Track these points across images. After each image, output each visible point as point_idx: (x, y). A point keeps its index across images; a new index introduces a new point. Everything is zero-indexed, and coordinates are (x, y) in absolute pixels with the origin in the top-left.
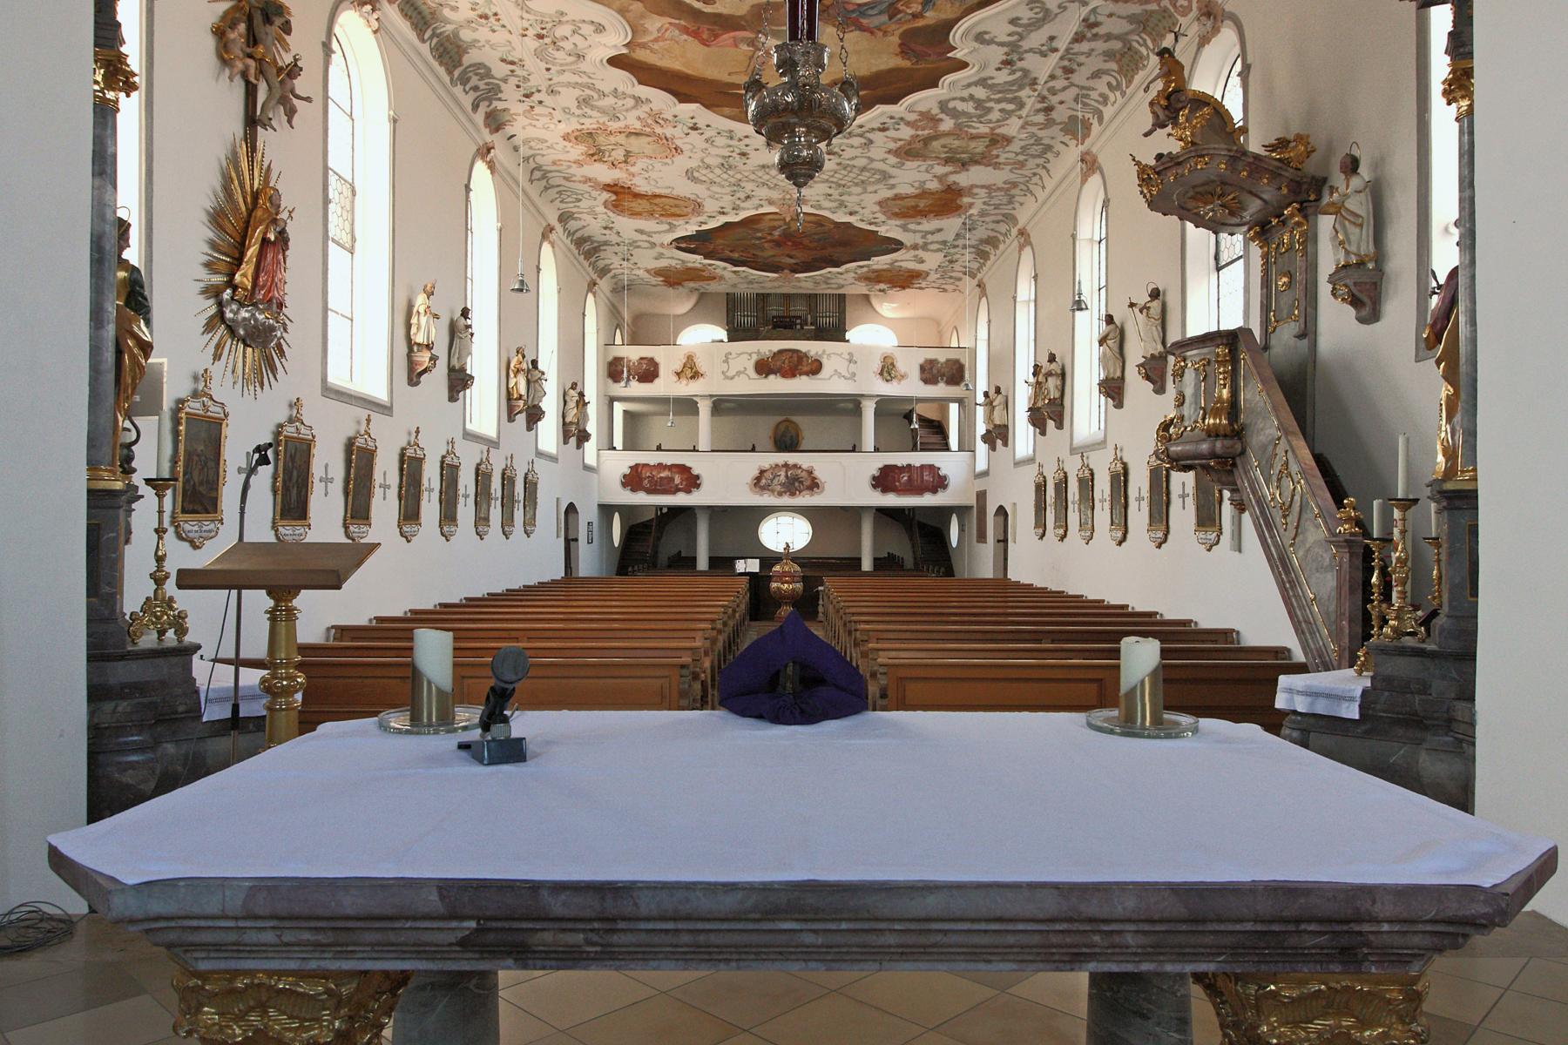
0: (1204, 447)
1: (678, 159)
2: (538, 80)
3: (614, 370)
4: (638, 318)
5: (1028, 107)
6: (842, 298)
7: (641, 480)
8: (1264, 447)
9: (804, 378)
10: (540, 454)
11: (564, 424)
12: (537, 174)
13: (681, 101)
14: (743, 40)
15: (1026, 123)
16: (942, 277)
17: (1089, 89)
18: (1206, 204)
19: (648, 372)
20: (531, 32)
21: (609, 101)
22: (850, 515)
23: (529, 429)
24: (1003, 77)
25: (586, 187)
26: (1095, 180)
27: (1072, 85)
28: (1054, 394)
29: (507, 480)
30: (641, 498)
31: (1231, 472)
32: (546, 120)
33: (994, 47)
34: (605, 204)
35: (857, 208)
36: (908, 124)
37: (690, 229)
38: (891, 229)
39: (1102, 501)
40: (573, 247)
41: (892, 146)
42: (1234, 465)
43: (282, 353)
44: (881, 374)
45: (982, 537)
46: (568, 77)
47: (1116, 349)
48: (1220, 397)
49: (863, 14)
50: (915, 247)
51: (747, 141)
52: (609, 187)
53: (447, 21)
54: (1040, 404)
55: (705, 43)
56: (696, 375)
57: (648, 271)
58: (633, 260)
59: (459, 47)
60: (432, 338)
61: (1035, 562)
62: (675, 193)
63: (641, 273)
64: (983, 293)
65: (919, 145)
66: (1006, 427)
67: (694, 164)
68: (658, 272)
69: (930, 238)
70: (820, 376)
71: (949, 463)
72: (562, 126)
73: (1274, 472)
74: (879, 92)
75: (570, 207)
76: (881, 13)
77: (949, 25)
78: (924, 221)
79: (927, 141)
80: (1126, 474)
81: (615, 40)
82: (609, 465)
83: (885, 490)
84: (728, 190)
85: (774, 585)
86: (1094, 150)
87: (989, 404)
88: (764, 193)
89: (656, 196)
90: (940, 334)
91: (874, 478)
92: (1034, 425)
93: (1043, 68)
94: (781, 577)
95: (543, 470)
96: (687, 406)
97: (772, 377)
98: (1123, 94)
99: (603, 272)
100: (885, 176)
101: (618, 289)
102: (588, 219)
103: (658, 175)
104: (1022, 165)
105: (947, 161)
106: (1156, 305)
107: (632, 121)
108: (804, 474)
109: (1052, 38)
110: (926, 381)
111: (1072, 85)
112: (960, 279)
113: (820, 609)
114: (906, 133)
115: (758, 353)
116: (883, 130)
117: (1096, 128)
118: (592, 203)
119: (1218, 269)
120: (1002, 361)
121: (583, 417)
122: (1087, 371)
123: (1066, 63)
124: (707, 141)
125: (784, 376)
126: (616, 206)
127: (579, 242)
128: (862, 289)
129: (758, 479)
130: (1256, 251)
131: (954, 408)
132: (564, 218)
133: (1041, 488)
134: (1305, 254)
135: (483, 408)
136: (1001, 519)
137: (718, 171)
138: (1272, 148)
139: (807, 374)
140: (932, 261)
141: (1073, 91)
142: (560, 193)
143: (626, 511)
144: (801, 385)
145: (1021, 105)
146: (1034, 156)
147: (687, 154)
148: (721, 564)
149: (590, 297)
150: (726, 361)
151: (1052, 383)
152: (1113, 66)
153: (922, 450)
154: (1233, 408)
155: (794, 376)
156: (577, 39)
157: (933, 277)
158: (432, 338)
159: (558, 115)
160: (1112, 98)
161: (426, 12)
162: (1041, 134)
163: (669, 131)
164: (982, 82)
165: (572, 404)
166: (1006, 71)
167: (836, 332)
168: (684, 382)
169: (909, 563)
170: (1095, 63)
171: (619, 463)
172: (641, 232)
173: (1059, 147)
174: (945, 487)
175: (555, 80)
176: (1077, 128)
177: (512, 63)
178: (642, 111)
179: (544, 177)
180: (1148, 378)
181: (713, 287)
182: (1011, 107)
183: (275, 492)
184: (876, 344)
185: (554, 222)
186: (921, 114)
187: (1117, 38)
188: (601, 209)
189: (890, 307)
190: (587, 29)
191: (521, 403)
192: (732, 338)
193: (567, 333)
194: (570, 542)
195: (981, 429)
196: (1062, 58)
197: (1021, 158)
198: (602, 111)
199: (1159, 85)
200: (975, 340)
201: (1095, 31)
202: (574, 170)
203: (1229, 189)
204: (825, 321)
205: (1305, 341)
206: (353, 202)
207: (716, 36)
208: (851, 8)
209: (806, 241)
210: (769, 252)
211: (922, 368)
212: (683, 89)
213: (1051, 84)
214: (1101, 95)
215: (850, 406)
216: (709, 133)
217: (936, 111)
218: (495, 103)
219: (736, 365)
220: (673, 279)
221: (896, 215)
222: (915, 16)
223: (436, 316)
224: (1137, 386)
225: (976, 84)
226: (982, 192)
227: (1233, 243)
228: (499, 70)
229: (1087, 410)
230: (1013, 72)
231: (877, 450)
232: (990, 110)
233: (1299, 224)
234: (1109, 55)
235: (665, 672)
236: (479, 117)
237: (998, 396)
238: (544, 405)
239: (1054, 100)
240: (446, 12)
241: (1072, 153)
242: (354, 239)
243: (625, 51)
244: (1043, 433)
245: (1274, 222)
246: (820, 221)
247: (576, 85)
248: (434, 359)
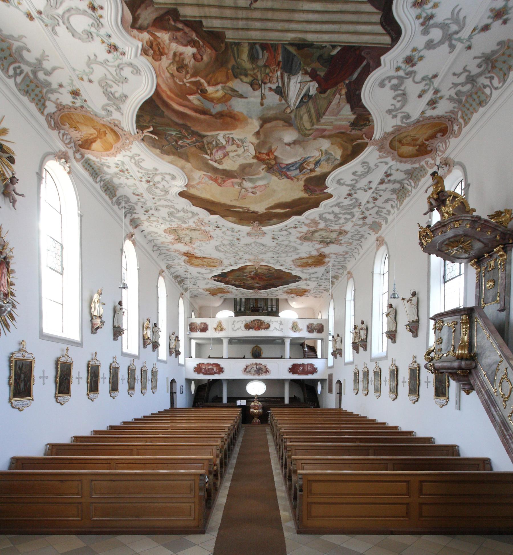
0: (456, 364)
1: (212, 241)
2: (150, 204)
3: (192, 328)
4: (201, 308)
5: (356, 217)
6: (277, 300)
7: (201, 369)
8: (490, 365)
9: (263, 330)
10: (158, 361)
11: (170, 348)
12: (156, 248)
13: (211, 214)
14: (237, 183)
15: (355, 225)
16: (316, 292)
17: (383, 208)
18: (453, 247)
19: (204, 329)
20: (144, 180)
21: (181, 214)
22: (281, 382)
23: (154, 351)
24: (347, 202)
25: (176, 254)
26: (383, 249)
27: (376, 206)
28: (363, 337)
29: (143, 372)
30: (201, 376)
31: (467, 376)
32: (155, 223)
33: (344, 186)
34: (184, 261)
35: (284, 263)
36: (306, 225)
37: (219, 272)
38: (296, 272)
39: (385, 381)
40: (173, 279)
41: (299, 235)
42: (470, 373)
43: (13, 318)
44: (292, 329)
45: (330, 391)
46: (163, 202)
47: (393, 318)
48: (463, 340)
49: (288, 170)
50: (306, 280)
51: (239, 233)
52: (186, 254)
53: (108, 174)
54: (357, 341)
55: (220, 185)
56: (222, 329)
57: (203, 289)
58: (197, 285)
59: (114, 187)
60: (102, 313)
61: (353, 403)
62: (212, 256)
63: (201, 290)
64: (332, 298)
65: (310, 235)
66: (341, 349)
67: (218, 243)
68: (208, 290)
69: (312, 276)
70: (269, 330)
71: (318, 363)
72: (163, 226)
73: (498, 378)
74: (295, 209)
75: (170, 263)
76: (296, 169)
77: (325, 176)
78: (310, 268)
79: (313, 233)
80: (397, 371)
81: (179, 184)
82: (188, 363)
83: (294, 373)
84: (232, 255)
85: (251, 410)
86: (383, 236)
87: (335, 341)
88: (247, 256)
89: (204, 258)
90: (314, 314)
91: (290, 369)
92: (354, 349)
93: (364, 197)
94: (254, 407)
95: (160, 368)
96: (219, 341)
97: (251, 330)
98: (398, 209)
99: (186, 290)
100: (296, 249)
101: (194, 296)
102: (178, 268)
103: (205, 249)
104: (351, 244)
105: (321, 242)
106: (414, 299)
107: (191, 223)
108: (263, 367)
109: (370, 182)
110: (309, 332)
111: (376, 206)
112: (322, 293)
113: (269, 419)
114: (305, 229)
115: (246, 321)
116: (295, 228)
117: (384, 226)
118: (179, 261)
119: (445, 282)
120: (340, 323)
121: (177, 346)
122: (379, 326)
123: (374, 195)
124: (223, 233)
125: (255, 330)
126: (189, 262)
127: (176, 277)
128: (285, 296)
129: (246, 369)
130: (473, 271)
131: (319, 342)
132: (169, 267)
133: (356, 374)
134: (505, 269)
135: (131, 342)
136: (338, 385)
137: (228, 247)
138: (492, 217)
139: (264, 329)
140: (312, 285)
141: (376, 209)
142: (166, 256)
143: (197, 381)
144: (262, 333)
145: (353, 216)
146: (356, 240)
147: (215, 239)
148: (232, 400)
149: (181, 300)
150: (233, 324)
151: (363, 333)
152: (394, 196)
153: (308, 358)
154: (470, 345)
155: (259, 330)
156: (164, 183)
157: (312, 292)
158: (102, 313)
159: (161, 221)
160: (392, 211)
161: (96, 168)
162: (360, 229)
163: (207, 229)
164: (338, 205)
165: (173, 341)
166: (348, 199)
167: (275, 313)
168: (218, 332)
169: (302, 400)
170: (387, 195)
171: (193, 363)
172: (199, 273)
173: (367, 235)
174: (316, 372)
175: (158, 204)
176: (376, 227)
177: (138, 195)
178: (195, 219)
179: (158, 249)
180: (411, 331)
181: (229, 296)
182: (348, 217)
183: (10, 385)
184: (290, 318)
185: (164, 268)
186: (312, 220)
187: (398, 182)
188: (183, 263)
189: (296, 304)
190: (168, 178)
191: (149, 341)
192: (236, 315)
193: (170, 313)
194: (173, 394)
195: (331, 350)
196: (373, 193)
197: (351, 241)
198: (179, 219)
199: (431, 190)
200: (329, 316)
201: (389, 178)
202: (170, 246)
203: (468, 238)
204: (271, 309)
205: (504, 313)
206: (62, 252)
207: (224, 181)
208: (283, 166)
209: (264, 277)
210: (250, 282)
211: (308, 327)
212: (212, 208)
213: (366, 206)
214: (387, 211)
215: (280, 341)
216: (224, 229)
217: (317, 219)
218: (134, 215)
219: (237, 326)
220: (213, 293)
221: (299, 266)
222: (312, 171)
223: (104, 304)
224: (403, 333)
225: (335, 205)
226: (334, 256)
227: (454, 268)
228: (134, 199)
229: (379, 344)
230: (352, 200)
231: (290, 358)
232: (340, 218)
233: (501, 256)
234: (393, 191)
235: (192, 478)
236: (127, 221)
237: (338, 338)
238: (160, 341)
239: (367, 213)
240: (105, 169)
241: (373, 237)
242: (63, 269)
243: (185, 189)
244: (358, 352)
245: (486, 256)
246: (269, 269)
247: (166, 206)
248: (103, 322)
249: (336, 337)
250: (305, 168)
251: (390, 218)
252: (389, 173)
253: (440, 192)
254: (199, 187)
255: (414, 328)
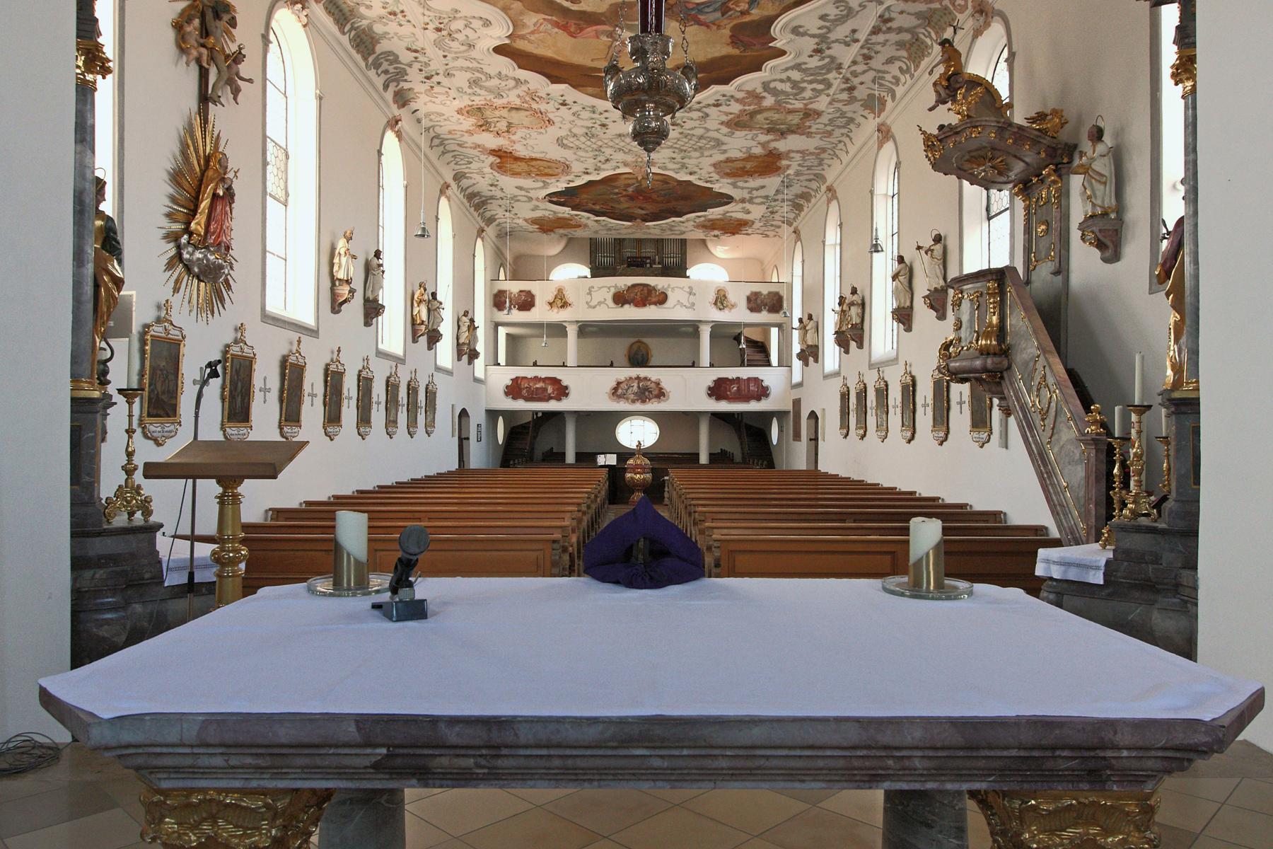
0: (978, 363)
1: (551, 129)
2: (436, 65)
3: (499, 301)
4: (518, 258)
5: (834, 87)
6: (683, 242)
7: (520, 390)
8: (1026, 364)
9: (653, 307)
10: (438, 369)
11: (458, 344)
12: (436, 142)
13: (553, 82)
14: (603, 32)
15: (833, 100)
16: (765, 225)
17: (884, 72)
19: (526, 302)
20: (431, 26)
21: (494, 82)
22: (690, 419)
23: (430, 348)
24: (814, 62)
25: (476, 152)
26: (889, 146)
27: (871, 69)
28: (856, 320)
29: (412, 390)
30: (520, 405)
31: (999, 384)
33: (807, 38)
34: (491, 166)
35: (696, 169)
36: (737, 100)
37: (560, 186)
38: (723, 186)
39: (895, 407)
40: (465, 201)
42: (1002, 378)
43: (229, 287)
44: (715, 304)
45: (797, 436)
46: (461, 63)
47: (906, 284)
48: (991, 322)
49: (701, 11)
50: (743, 201)
51: (606, 115)
52: (494, 152)
53: (363, 17)
54: (844, 328)
55: (572, 35)
56: (565, 305)
57: (526, 220)
58: (514, 211)
59: (372, 38)
60: (351, 274)
61: (840, 456)
63: (520, 222)
64: (798, 238)
65: (746, 118)
66: (817, 347)
67: (563, 133)
68: (534, 221)
69: (755, 193)
70: (666, 305)
71: (770, 376)
72: (456, 103)
73: (1035, 383)
74: (714, 75)
75: (463, 168)
76: (715, 10)
77: (770, 20)
78: (750, 179)
79: (752, 114)
80: (914, 385)
81: (499, 33)
82: (494, 378)
83: (718, 398)
84: (591, 154)
85: (628, 475)
86: (888, 122)
87: (803, 328)
88: (620, 156)
89: (532, 159)
90: (763, 271)
91: (710, 388)
92: (839, 345)
93: (847, 55)
94: (634, 469)
95: (441, 382)
96: (558, 330)
97: (627, 306)
98: (912, 76)
99: (490, 221)
100: (719, 143)
101: (502, 235)
102: (478, 178)
103: (534, 142)
104: (830, 134)
106: (938, 248)
107: (513, 98)
108: (653, 385)
109: (854, 31)
110: (752, 310)
111: (871, 69)
112: (779, 227)
113: (666, 495)
114: (736, 108)
115: (616, 286)
116: (717, 105)
117: (889, 104)
118: (481, 165)
119: (989, 219)
120: (813, 293)
121: (474, 338)
123: (865, 51)
124: (574, 114)
125: (636, 305)
126: (500, 168)
127: (470, 197)
128: (700, 234)
129: (616, 389)
130: (1020, 204)
131: (774, 332)
132: (458, 177)
133: (845, 397)
134: (1060, 206)
135: (392, 332)
136: (813, 421)
137: (583, 139)
138: (1033, 120)
139: (655, 304)
140: (757, 212)
141: (871, 74)
142: (454, 156)
143: (509, 415)
144: (651, 313)
145: (829, 85)
146: (839, 127)
147: (558, 125)
148: (586, 458)
149: (479, 241)
150: (590, 293)
151: (854, 311)
152: (904, 53)
153: (749, 366)
154: (1001, 331)
155: (644, 305)
156: (468, 32)
157: (757, 225)
158: (351, 274)
159: (453, 93)
160: (903, 80)
161: (346, 10)
162: (845, 109)
163: (543, 107)
164: (798, 67)
165: (464, 328)
166: (816, 58)
167: (678, 270)
168: (555, 310)
169: (738, 457)
170: (889, 51)
171: (503, 376)
172: (520, 188)
173: (859, 119)
174: (767, 396)
175: (451, 65)
176: (874, 104)
177: (416, 51)
178: (521, 90)
179: (441, 144)
180: (932, 307)
181: (579, 233)
182: (821, 87)
183: (223, 399)
184: (711, 280)
185: (450, 180)
186: (748, 92)
187: (907, 31)
188: (488, 170)
189: (723, 249)
190: (477, 24)
191: (423, 327)
192: (595, 275)
193: (460, 271)
194: (463, 441)
195: (796, 348)
196: (862, 47)
197: (829, 128)
198: (489, 90)
199: (941, 69)
200: (792, 277)
201: (889, 25)
202: (466, 138)
203: (998, 153)
204: (669, 261)
205: (1060, 277)
206: (286, 164)
207: (581, 30)
208: (691, 6)
209: (654, 196)
210: (624, 205)
211: (749, 299)
212: (555, 73)
213: (853, 68)
215: (690, 330)
216: (575, 108)
217: (760, 90)
218: (402, 84)
219: (598, 296)
220: (546, 226)
221: (728, 175)
222: (743, 13)
223: (354, 257)
224: (923, 314)
225: (792, 68)
226: (798, 156)
227: (1001, 198)
228: (405, 57)
229: (883, 333)
230: (823, 59)
231: (712, 365)
232: (804, 89)
233: (1054, 182)
234: (901, 45)
235: (540, 546)
236: (389, 95)
237: (811, 322)
238: (442, 329)
239: (856, 81)
240: (362, 10)
241: (871, 124)
242: (287, 194)
243: (507, 41)
244: (847, 352)
245: (1035, 180)
246: (666, 180)
247: (467, 69)
248: (352, 291)
249: (805, 320)
250: (731, 9)
251: (899, 91)
252: (887, 15)
253: (953, 74)
254: (532, 38)
255: (937, 302)
